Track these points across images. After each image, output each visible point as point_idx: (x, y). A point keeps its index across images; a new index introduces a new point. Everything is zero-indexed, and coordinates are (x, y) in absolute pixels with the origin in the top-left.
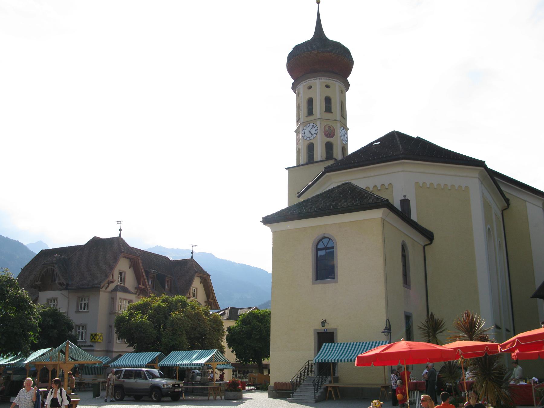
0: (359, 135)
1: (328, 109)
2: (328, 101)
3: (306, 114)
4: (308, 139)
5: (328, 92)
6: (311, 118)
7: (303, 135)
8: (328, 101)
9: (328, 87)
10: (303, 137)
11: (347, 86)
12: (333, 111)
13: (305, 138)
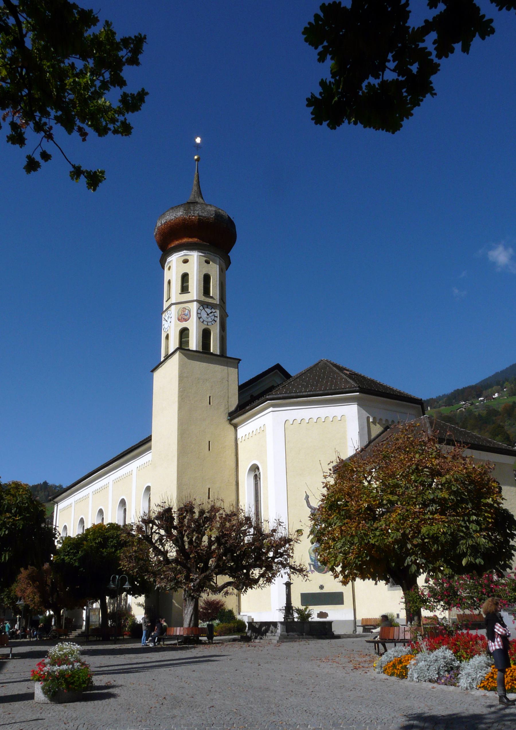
6: (185, 297)
7: (200, 316)
9: (207, 262)
10: (200, 318)
13: (201, 320)
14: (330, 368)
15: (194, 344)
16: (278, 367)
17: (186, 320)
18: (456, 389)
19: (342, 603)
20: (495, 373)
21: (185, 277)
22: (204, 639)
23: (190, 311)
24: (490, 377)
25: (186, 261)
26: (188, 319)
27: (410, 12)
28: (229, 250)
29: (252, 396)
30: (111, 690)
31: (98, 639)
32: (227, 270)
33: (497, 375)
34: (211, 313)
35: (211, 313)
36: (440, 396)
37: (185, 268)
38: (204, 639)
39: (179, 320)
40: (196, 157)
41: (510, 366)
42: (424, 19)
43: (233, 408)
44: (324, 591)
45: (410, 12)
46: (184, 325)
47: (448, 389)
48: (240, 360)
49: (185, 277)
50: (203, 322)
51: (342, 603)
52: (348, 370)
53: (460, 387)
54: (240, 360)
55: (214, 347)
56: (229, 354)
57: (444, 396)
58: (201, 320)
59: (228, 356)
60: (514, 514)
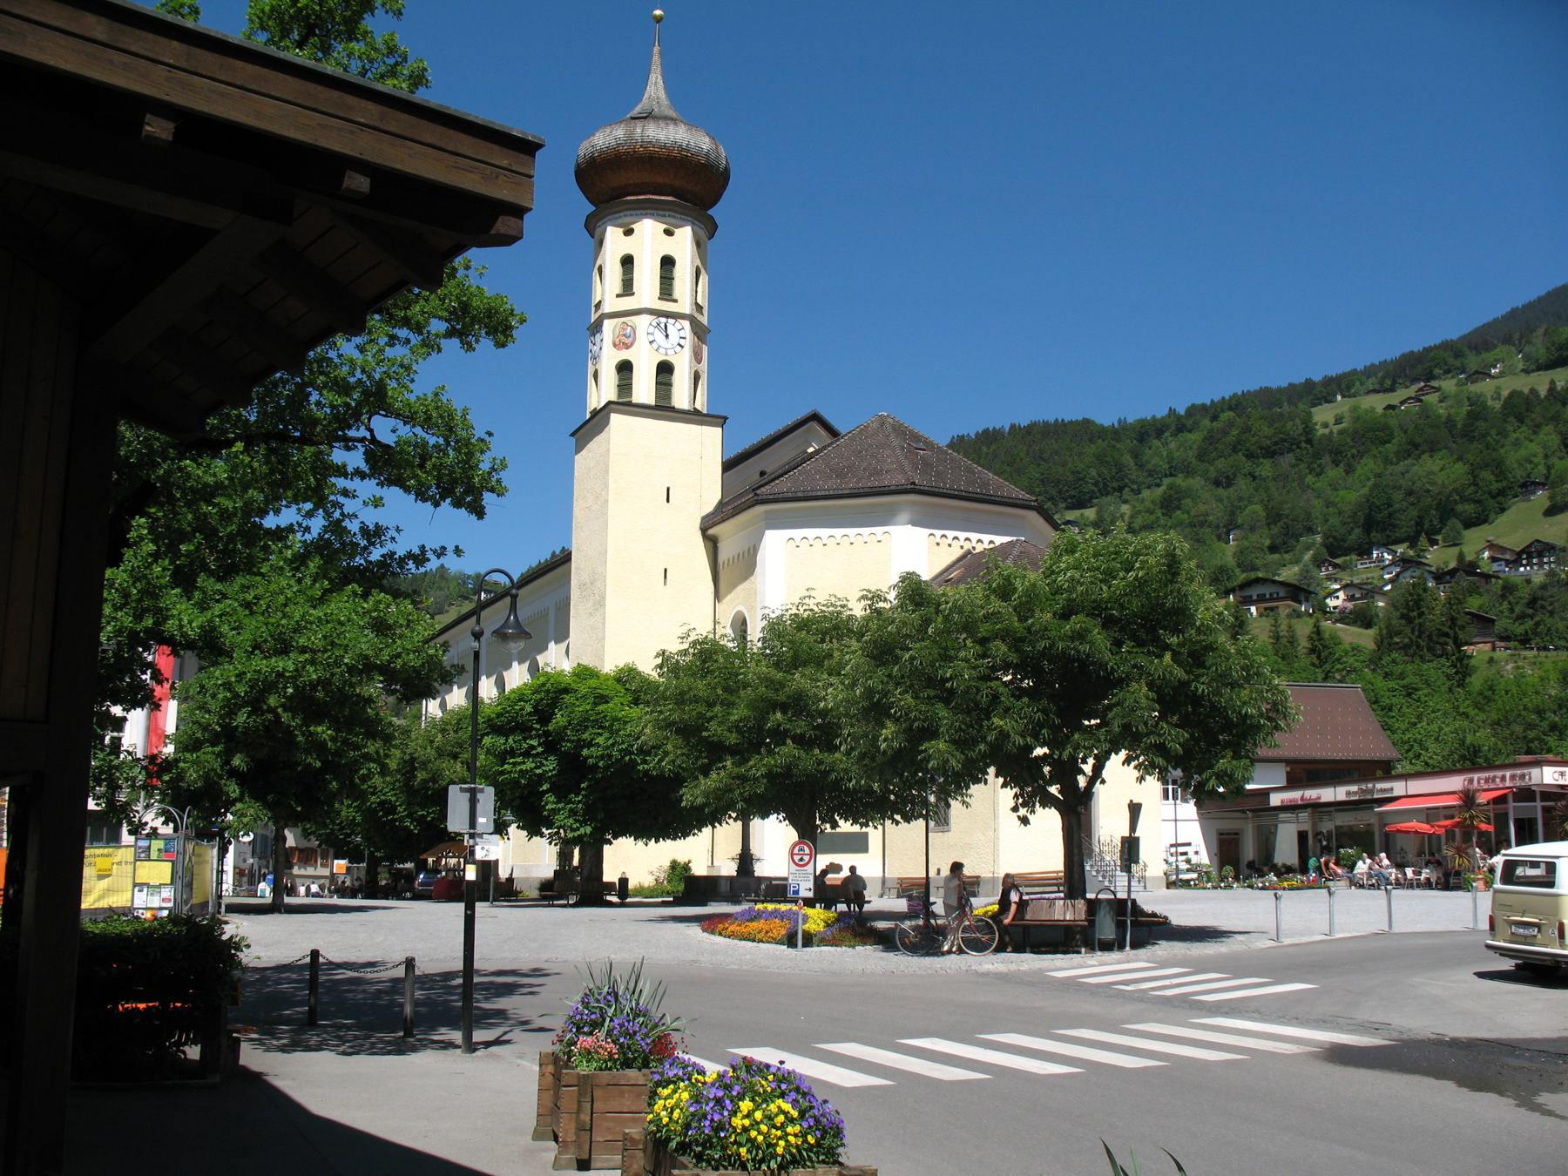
9: (669, 233)
12: (676, 295)
13: (655, 345)
16: (815, 417)
17: (628, 347)
18: (1406, 350)
19: (866, 850)
20: (1508, 309)
22: (615, 899)
24: (1496, 321)
29: (762, 474)
30: (502, 1003)
33: (1513, 314)
36: (1373, 365)
38: (615, 899)
40: (658, 12)
41: (1548, 294)
42: (663, 358)
43: (709, 507)
46: (624, 355)
47: (1390, 349)
51: (866, 850)
53: (1417, 347)
54: (726, 418)
57: (1384, 363)
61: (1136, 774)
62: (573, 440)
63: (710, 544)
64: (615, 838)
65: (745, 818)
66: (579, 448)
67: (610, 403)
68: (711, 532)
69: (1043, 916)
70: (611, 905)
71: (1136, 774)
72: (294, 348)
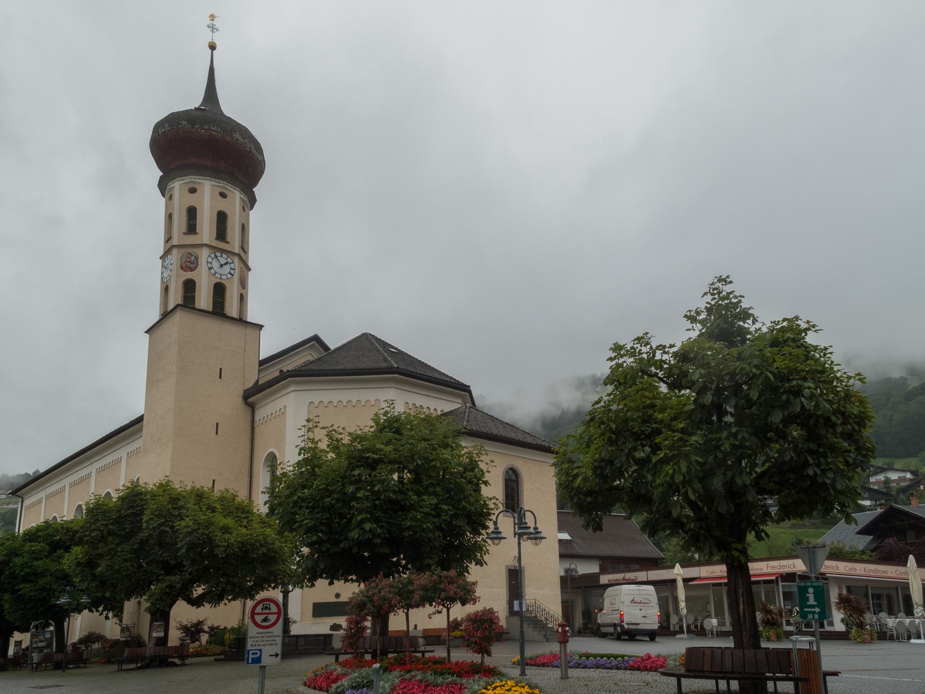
0: (280, 315)
1: (221, 233)
2: (222, 218)
3: (184, 229)
4: (217, 275)
5: (222, 205)
6: (191, 239)
7: (210, 266)
8: (222, 218)
9: (223, 195)
10: (210, 269)
11: (252, 201)
12: (229, 238)
13: (213, 272)
14: (373, 344)
15: (204, 300)
16: (316, 338)
17: (192, 270)
21: (192, 213)
23: (197, 258)
25: (193, 191)
26: (195, 269)
27: (475, 584)
28: (255, 182)
31: (139, 665)
32: (251, 208)
34: (226, 263)
35: (226, 263)
37: (192, 200)
39: (182, 268)
44: (340, 600)
45: (475, 584)
46: (189, 275)
48: (262, 326)
49: (192, 213)
50: (210, 269)
52: (393, 347)
54: (262, 326)
55: (232, 309)
56: (673, 680)
58: (213, 272)
59: (249, 320)
60: (218, 608)
61: (327, 581)
62: (147, 335)
63: (250, 409)
64: (903, 380)
65: (284, 585)
66: (142, 416)
67: (178, 305)
68: (250, 400)
69: (656, 619)
70: (174, 665)
71: (327, 581)
72: (125, 641)
